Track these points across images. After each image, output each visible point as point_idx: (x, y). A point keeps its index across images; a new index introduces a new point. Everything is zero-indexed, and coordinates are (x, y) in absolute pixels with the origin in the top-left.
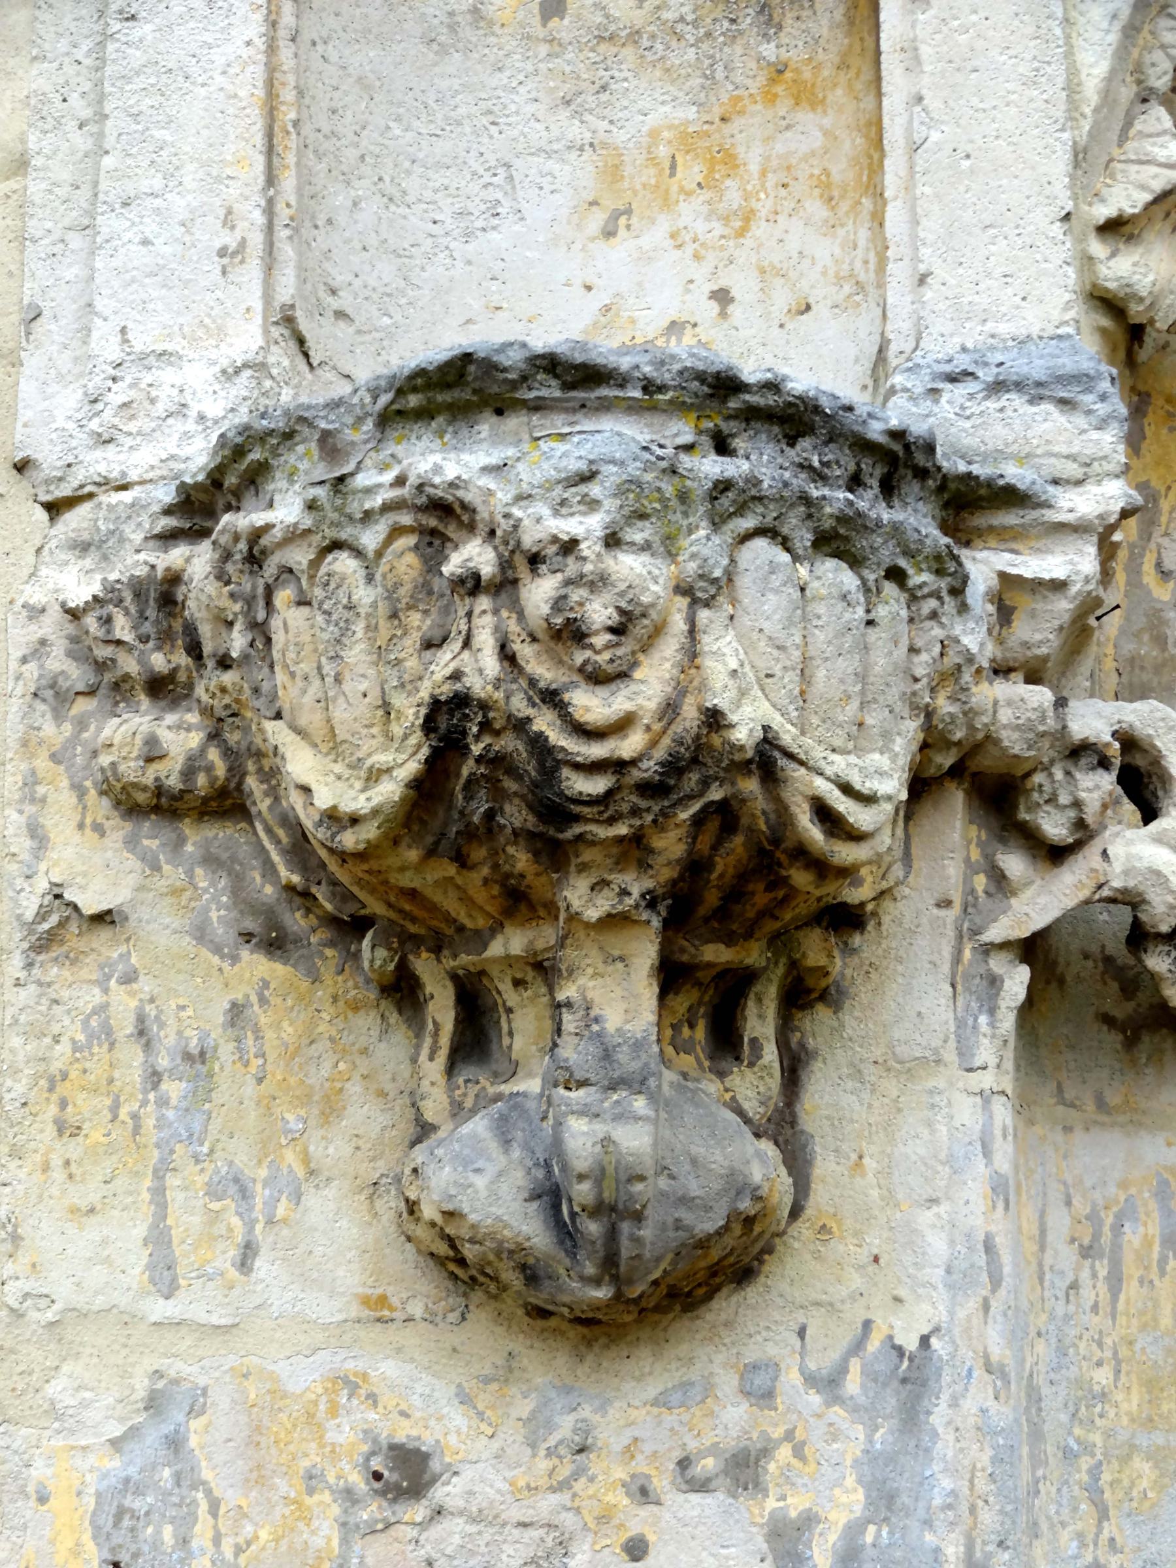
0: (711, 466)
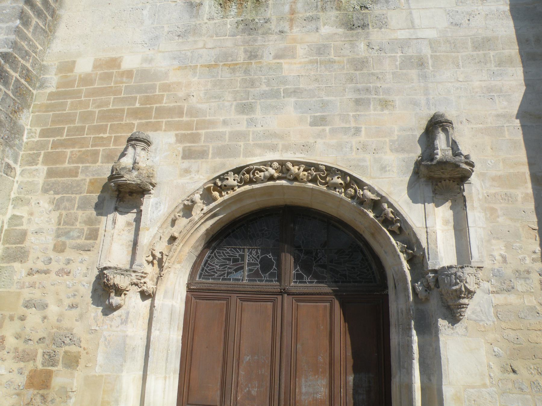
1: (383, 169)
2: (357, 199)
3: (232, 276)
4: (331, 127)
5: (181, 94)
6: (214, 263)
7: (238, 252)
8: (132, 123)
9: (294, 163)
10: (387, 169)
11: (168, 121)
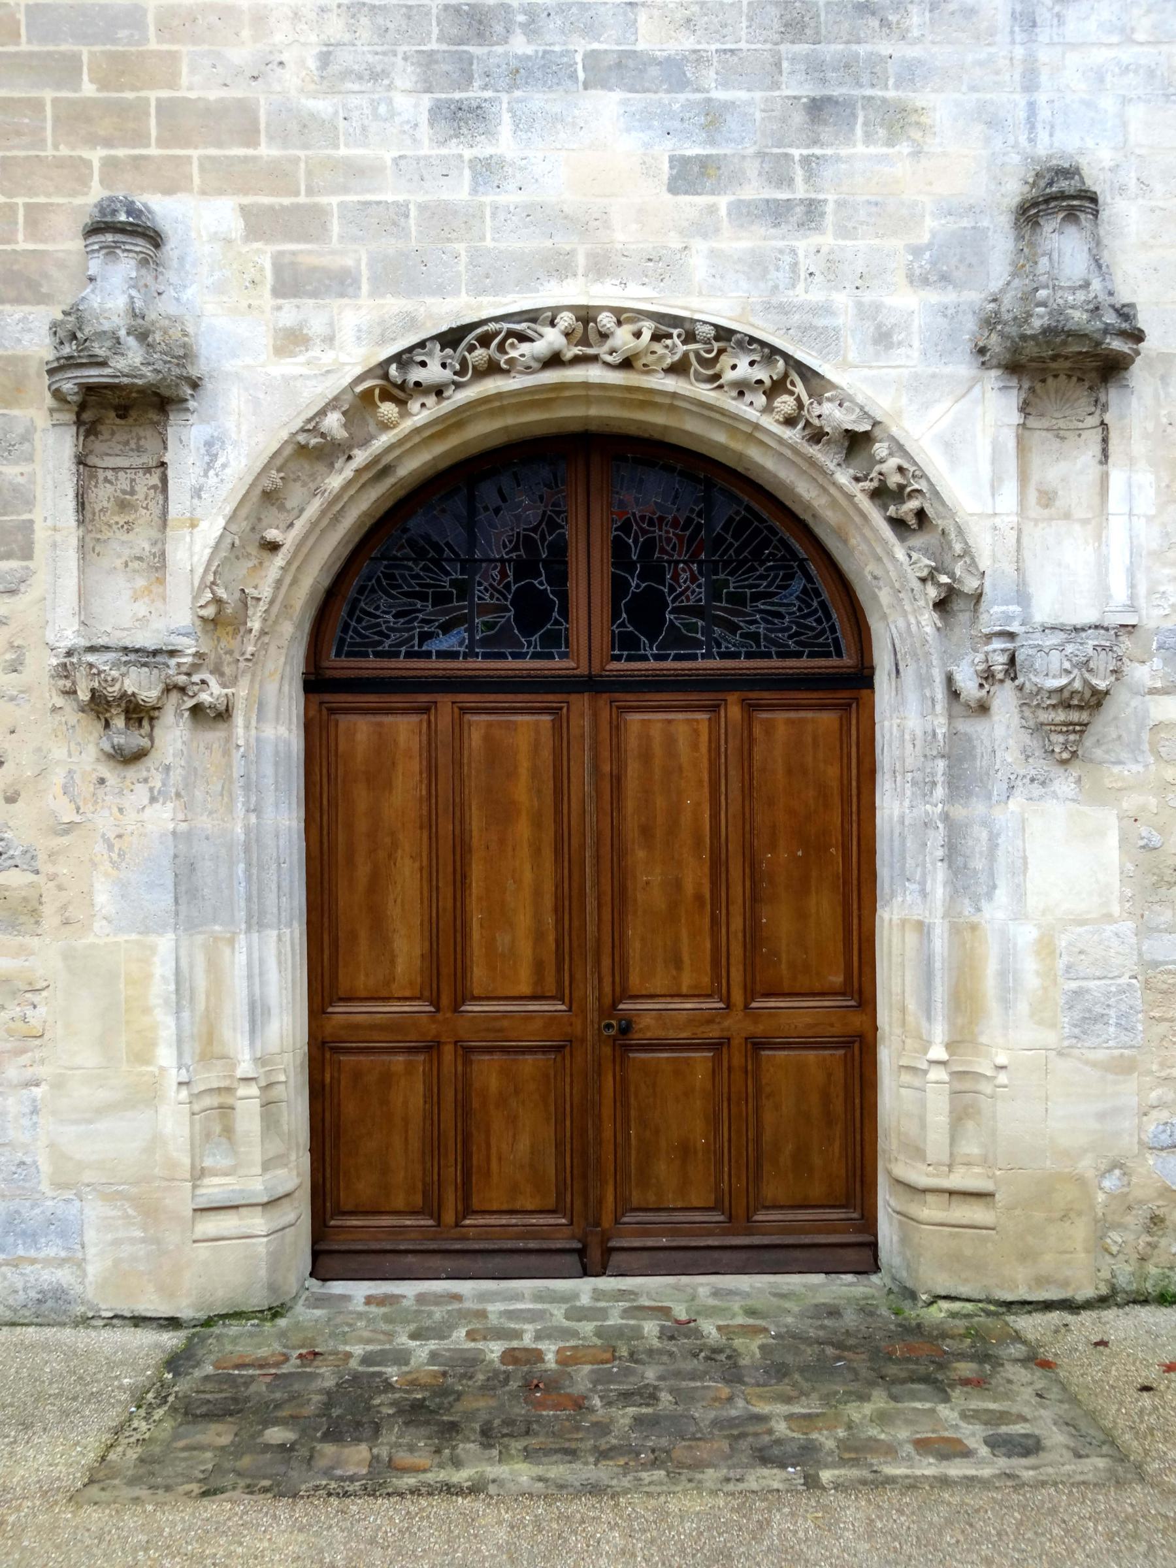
0: (125, 659)
1: (884, 338)
2: (804, 428)
3: (433, 646)
4: (732, 198)
5: (241, 54)
6: (377, 608)
7: (447, 574)
8: (81, 158)
9: (621, 315)
10: (895, 338)
11: (209, 157)
